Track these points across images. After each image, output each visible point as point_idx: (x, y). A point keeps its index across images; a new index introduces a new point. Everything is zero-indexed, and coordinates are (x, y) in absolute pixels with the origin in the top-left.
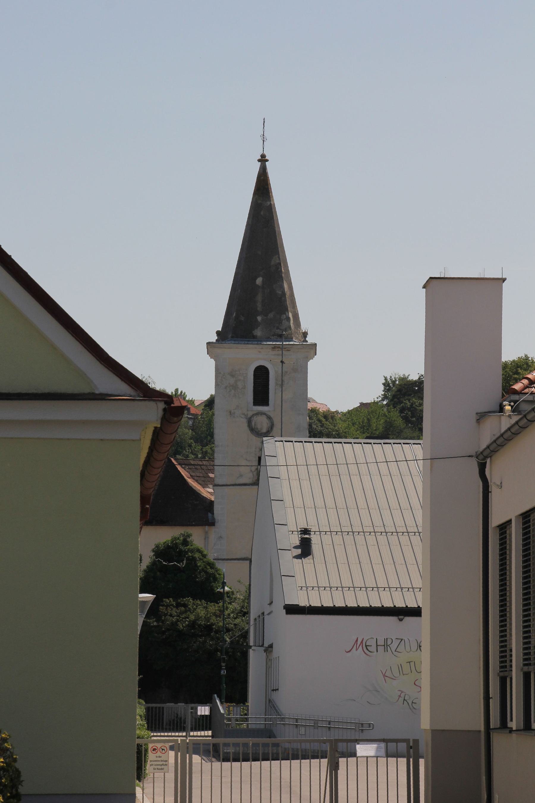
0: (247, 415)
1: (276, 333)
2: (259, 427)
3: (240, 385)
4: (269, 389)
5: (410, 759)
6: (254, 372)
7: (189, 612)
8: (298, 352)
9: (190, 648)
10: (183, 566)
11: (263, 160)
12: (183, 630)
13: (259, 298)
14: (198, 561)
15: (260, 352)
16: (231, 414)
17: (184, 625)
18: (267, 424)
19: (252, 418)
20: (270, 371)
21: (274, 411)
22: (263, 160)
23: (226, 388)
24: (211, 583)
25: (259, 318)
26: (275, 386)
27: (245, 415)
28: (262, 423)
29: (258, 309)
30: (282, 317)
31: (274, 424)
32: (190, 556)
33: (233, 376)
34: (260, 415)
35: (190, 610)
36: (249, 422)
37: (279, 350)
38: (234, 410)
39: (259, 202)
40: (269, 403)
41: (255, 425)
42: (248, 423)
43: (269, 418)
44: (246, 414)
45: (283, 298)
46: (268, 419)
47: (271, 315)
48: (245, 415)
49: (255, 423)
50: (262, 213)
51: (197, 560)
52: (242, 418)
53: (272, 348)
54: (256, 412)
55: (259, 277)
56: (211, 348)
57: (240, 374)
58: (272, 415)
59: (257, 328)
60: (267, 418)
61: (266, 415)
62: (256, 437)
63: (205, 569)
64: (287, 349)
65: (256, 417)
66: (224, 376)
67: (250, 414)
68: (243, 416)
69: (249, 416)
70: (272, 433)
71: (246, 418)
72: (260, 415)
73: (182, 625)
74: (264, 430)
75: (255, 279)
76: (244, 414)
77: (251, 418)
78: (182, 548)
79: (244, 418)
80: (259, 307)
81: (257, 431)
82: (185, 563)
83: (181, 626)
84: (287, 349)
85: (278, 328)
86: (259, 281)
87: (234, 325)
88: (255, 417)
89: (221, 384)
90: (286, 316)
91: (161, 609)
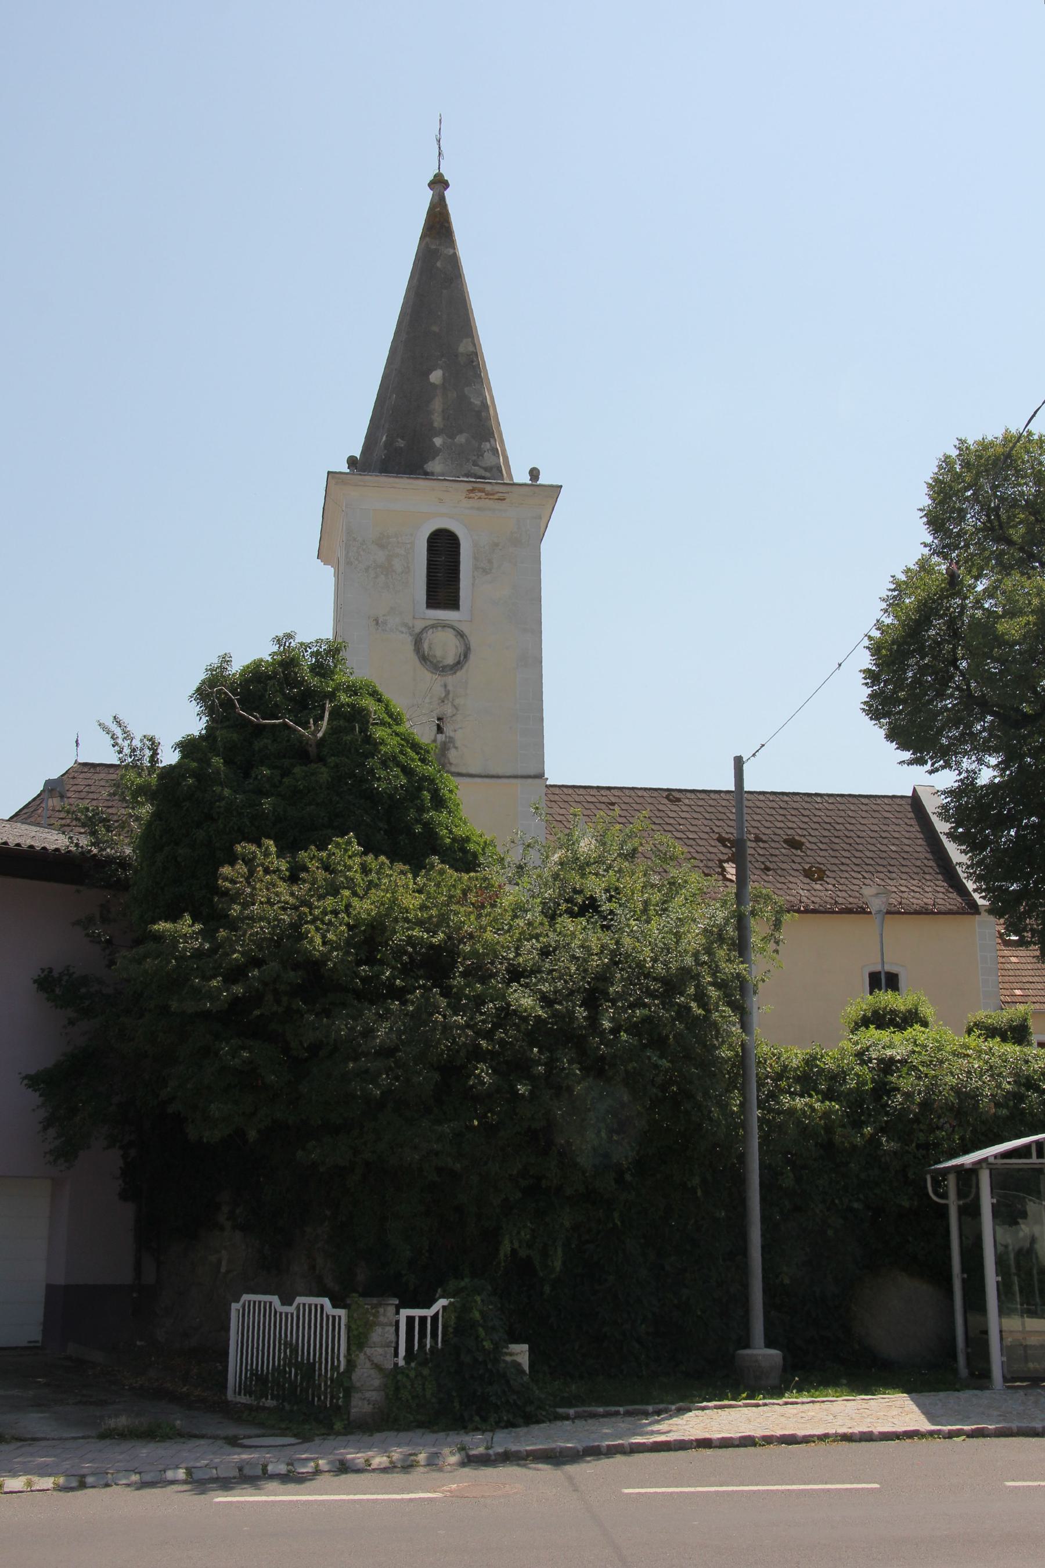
0: (413, 627)
1: (472, 471)
2: (439, 653)
3: (398, 565)
4: (459, 588)
5: (524, 1342)
6: (428, 541)
7: (347, 893)
8: (522, 504)
9: (435, 920)
10: (320, 735)
11: (439, 183)
12: (326, 957)
13: (437, 405)
14: (373, 724)
15: (441, 501)
16: (377, 623)
17: (330, 936)
18: (457, 647)
19: (424, 635)
20: (461, 542)
21: (471, 621)
22: (439, 183)
23: (367, 569)
24: (421, 810)
25: (438, 441)
26: (473, 572)
27: (409, 628)
28: (444, 646)
29: (436, 425)
30: (482, 446)
31: (471, 647)
32: (343, 705)
33: (382, 547)
34: (440, 628)
35: (351, 885)
36: (418, 642)
37: (480, 498)
38: (384, 615)
39: (433, 247)
40: (461, 604)
41: (430, 648)
42: (415, 644)
43: (461, 635)
44: (411, 625)
45: (483, 414)
46: (459, 637)
47: (461, 439)
48: (409, 628)
49: (430, 644)
50: (439, 264)
51: (371, 721)
52: (402, 633)
53: (468, 490)
54: (431, 622)
55: (435, 370)
56: (337, 484)
57: (398, 543)
58: (465, 628)
59: (434, 458)
60: (456, 636)
61: (454, 629)
62: (432, 673)
63: (402, 758)
64: (496, 497)
65: (433, 633)
66: (364, 547)
67: (419, 625)
68: (404, 629)
69: (417, 630)
70: (467, 665)
71: (411, 635)
72: (440, 628)
73: (324, 937)
74: (450, 660)
75: (430, 371)
76: (406, 625)
77: (421, 633)
78: (314, 681)
79: (406, 633)
80: (438, 421)
81: (435, 661)
82: (323, 729)
83: (318, 940)
84: (496, 497)
85: (475, 464)
86: (436, 376)
87: (383, 457)
88: (431, 630)
89: (357, 562)
90: (491, 445)
91: (226, 879)
